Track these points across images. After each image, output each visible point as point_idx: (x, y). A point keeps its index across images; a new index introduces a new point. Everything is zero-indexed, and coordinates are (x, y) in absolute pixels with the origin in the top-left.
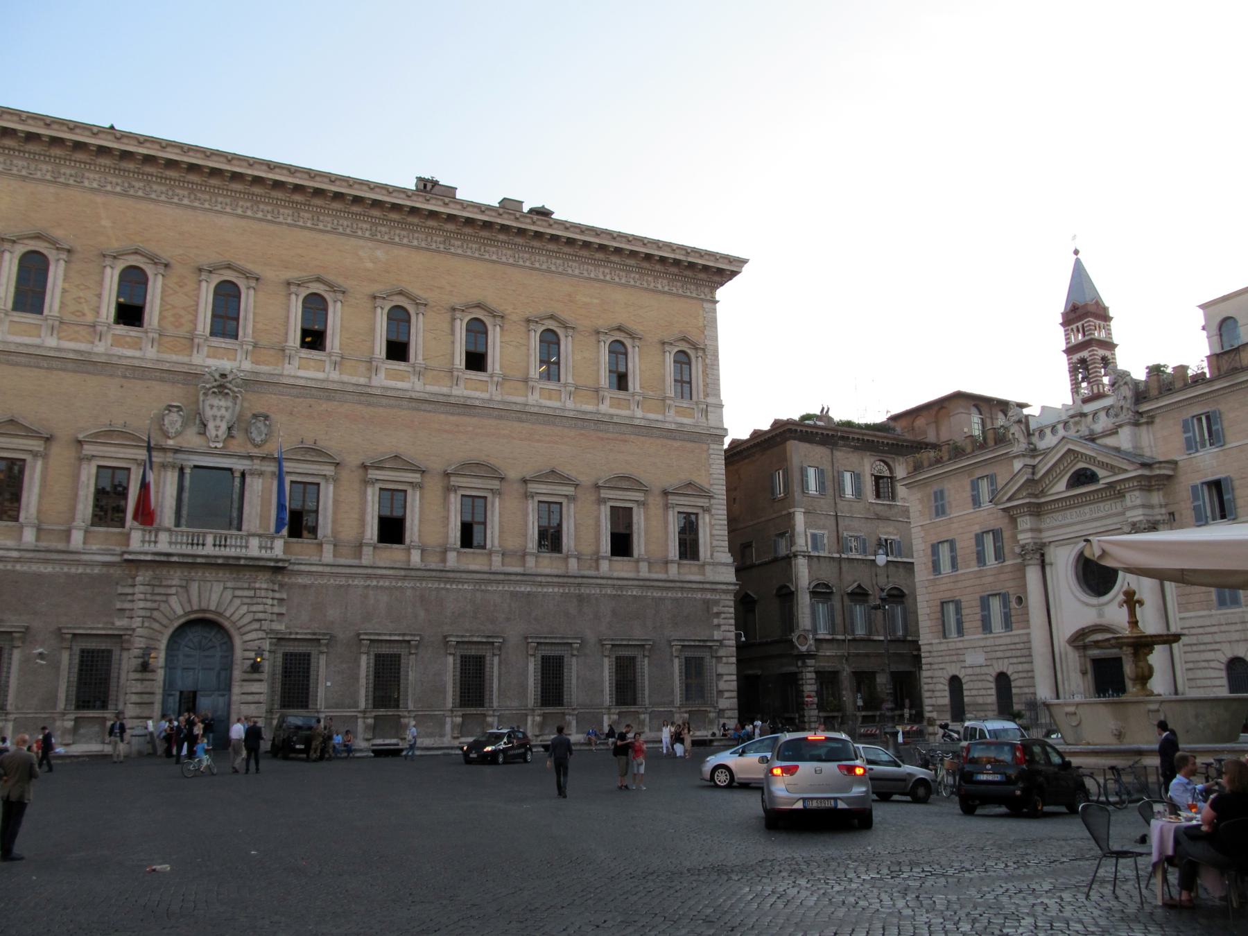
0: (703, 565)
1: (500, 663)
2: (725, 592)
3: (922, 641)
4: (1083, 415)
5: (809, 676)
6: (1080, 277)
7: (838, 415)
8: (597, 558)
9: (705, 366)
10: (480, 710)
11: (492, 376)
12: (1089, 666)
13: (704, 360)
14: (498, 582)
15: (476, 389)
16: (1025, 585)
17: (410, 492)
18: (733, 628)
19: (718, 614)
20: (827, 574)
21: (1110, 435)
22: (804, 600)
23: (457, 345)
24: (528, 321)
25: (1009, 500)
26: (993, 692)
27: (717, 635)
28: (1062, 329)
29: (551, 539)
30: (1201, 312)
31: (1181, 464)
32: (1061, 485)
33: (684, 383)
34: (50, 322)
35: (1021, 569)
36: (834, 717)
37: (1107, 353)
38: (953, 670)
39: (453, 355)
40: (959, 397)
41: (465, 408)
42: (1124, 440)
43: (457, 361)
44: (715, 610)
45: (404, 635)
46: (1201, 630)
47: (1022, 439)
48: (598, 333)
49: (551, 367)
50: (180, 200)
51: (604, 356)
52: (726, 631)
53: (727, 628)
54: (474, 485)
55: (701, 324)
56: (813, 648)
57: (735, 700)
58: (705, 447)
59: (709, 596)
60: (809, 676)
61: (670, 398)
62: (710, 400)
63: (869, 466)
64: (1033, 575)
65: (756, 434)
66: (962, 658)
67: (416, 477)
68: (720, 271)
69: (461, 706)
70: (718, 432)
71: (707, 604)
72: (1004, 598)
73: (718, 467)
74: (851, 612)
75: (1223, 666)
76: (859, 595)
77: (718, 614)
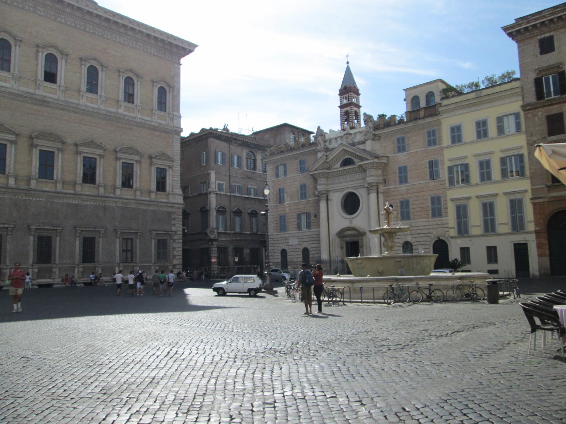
1: (60, 240)
2: (178, 208)
3: (270, 233)
4: (350, 134)
5: (214, 249)
6: (348, 75)
7: (233, 129)
8: (115, 188)
9: (173, 96)
10: (49, 265)
11: (59, 86)
12: (344, 245)
13: (173, 93)
14: (60, 198)
15: (50, 93)
16: (319, 209)
17: (9, 145)
18: (181, 226)
19: (174, 219)
20: (225, 203)
21: (361, 144)
22: (213, 214)
23: (40, 66)
24: (81, 59)
25: (315, 170)
26: (301, 256)
27: (174, 229)
28: (339, 97)
29: (89, 176)
30: (404, 93)
31: (390, 158)
32: (338, 165)
33: (162, 105)
35: (317, 202)
36: (224, 268)
37: (357, 109)
38: (283, 247)
39: (37, 72)
40: (285, 125)
41: (44, 102)
42: (369, 146)
43: (39, 76)
44: (173, 216)
45: (4, 224)
46: (424, 228)
47: (322, 143)
48: (119, 71)
51: (122, 85)
52: (178, 227)
53: (178, 225)
54: (47, 145)
56: (217, 236)
57: (181, 260)
60: (214, 249)
61: (155, 110)
62: (175, 113)
63: (244, 153)
64: (323, 205)
65: (192, 134)
66: (287, 241)
67: (12, 137)
68: (184, 49)
69: (38, 263)
70: (178, 130)
71: (169, 213)
72: (308, 215)
73: (177, 147)
74: (234, 221)
75: (401, 245)
76: (238, 213)
77: (174, 219)
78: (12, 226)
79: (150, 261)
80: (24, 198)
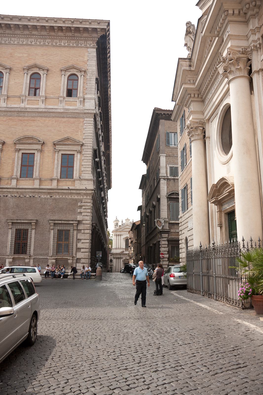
0: (75, 181)
2: (86, 194)
19: (81, 207)
27: (79, 218)
30: (198, 7)
34: (42, 98)
49: (34, 90)
54: (67, 149)
55: (86, 59)
58: (81, 120)
59: (76, 197)
77: (81, 207)
78: (35, 221)
79: (47, 254)
80: (45, 196)
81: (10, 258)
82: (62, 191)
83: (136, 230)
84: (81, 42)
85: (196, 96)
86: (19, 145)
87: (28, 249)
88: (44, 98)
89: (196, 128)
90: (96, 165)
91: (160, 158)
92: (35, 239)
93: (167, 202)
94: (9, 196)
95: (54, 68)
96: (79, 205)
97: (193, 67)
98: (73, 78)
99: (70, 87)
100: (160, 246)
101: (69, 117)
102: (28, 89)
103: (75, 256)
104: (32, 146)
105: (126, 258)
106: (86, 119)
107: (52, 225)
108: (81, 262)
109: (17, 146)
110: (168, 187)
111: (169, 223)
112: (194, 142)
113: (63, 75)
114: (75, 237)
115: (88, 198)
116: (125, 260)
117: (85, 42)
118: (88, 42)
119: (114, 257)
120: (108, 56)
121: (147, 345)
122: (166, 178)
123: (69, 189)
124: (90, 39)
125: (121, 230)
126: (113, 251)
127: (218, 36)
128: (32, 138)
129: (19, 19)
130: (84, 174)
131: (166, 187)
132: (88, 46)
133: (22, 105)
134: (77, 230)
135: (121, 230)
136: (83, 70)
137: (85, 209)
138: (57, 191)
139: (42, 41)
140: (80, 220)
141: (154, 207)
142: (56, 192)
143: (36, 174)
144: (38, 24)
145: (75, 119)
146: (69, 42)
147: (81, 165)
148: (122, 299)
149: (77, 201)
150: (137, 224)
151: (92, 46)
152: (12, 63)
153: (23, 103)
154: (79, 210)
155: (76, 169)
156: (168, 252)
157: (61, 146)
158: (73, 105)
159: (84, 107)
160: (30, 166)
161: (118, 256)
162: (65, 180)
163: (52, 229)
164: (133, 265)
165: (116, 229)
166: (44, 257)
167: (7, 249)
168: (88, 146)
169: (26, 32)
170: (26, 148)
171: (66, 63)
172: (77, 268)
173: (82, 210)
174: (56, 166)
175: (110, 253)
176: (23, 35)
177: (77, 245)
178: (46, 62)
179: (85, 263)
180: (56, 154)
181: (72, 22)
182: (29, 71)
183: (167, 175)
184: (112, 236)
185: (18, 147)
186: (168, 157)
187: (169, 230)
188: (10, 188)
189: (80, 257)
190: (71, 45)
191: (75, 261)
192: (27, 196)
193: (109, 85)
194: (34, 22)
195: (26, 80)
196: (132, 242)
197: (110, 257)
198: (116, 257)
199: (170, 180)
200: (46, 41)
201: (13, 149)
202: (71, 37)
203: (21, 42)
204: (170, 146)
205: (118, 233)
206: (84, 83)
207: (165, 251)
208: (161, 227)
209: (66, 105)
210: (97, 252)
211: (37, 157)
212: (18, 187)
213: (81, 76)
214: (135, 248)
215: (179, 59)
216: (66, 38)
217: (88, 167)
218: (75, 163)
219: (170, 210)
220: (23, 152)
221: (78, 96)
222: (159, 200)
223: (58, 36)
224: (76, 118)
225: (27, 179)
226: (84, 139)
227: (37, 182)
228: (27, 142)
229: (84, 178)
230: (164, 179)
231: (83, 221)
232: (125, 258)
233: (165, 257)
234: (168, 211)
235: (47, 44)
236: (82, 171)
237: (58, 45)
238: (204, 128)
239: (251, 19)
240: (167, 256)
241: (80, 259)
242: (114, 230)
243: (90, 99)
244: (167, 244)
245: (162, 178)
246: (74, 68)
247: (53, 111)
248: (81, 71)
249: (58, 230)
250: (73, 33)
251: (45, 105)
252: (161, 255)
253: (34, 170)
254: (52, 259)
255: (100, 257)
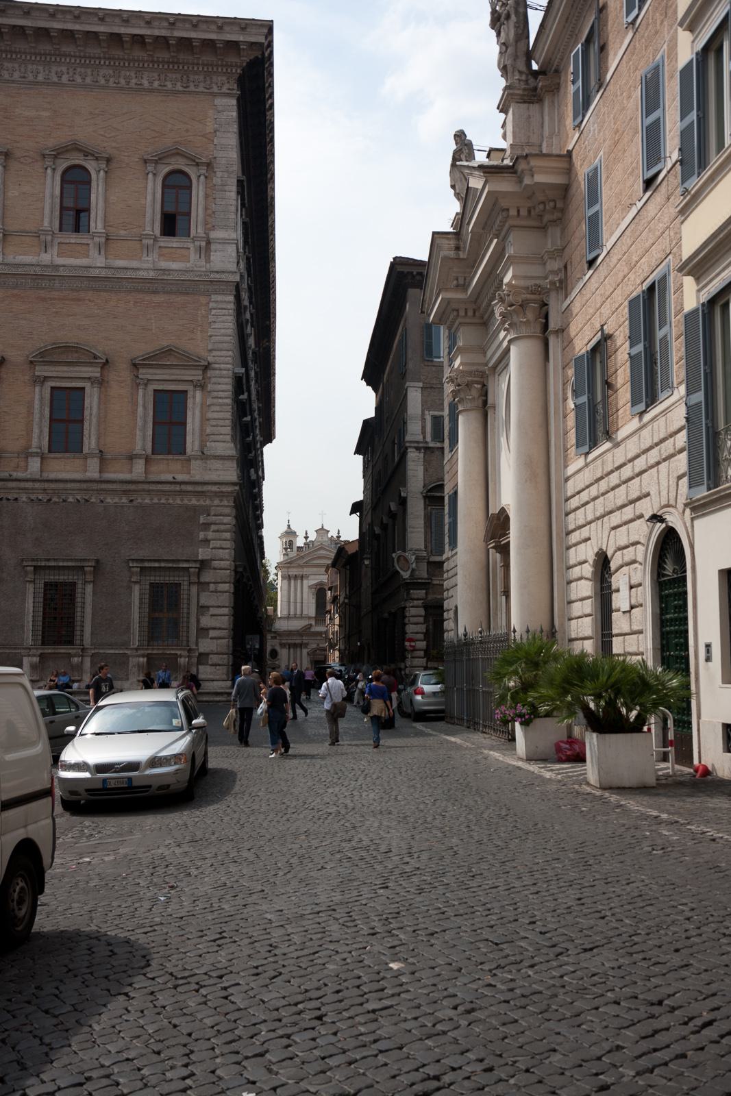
0: (189, 460)
19: (206, 526)
27: (203, 553)
34: (97, 240)
49: (75, 216)
50: (220, 88)
54: (165, 379)
55: (210, 129)
58: (203, 300)
59: (194, 502)
77: (206, 526)
79: (125, 644)
80: (116, 500)
81: (34, 656)
82: (160, 486)
83: (348, 567)
84: (197, 77)
85: (470, 313)
86: (43, 367)
87: (78, 633)
88: (103, 240)
89: (469, 385)
90: (241, 408)
91: (406, 394)
92: (94, 607)
93: (425, 509)
94: (24, 499)
95: (126, 154)
96: (201, 522)
97: (464, 251)
98: (177, 184)
99: (170, 209)
100: (406, 620)
101: (171, 293)
102: (57, 213)
103: (194, 647)
104: (77, 369)
105: (318, 645)
106: (214, 298)
107: (137, 572)
108: (210, 663)
109: (37, 368)
110: (426, 470)
111: (429, 563)
112: (464, 413)
113: (150, 176)
114: (194, 601)
115: (225, 503)
116: (314, 651)
117: (208, 78)
118: (214, 78)
119: (283, 641)
120: (267, 106)
121: (390, 916)
122: (421, 445)
123: (175, 483)
124: (220, 70)
125: (301, 562)
126: (281, 625)
127: (497, 236)
128: (75, 349)
129: (25, 12)
130: (213, 444)
131: (421, 469)
132: (215, 89)
133: (45, 258)
134: (199, 583)
135: (301, 562)
136: (204, 160)
137: (218, 531)
138: (146, 487)
139: (89, 71)
140: (206, 560)
141: (393, 516)
142: (144, 490)
143: (90, 442)
144: (77, 27)
145: (186, 298)
146: (162, 77)
147: (204, 420)
148: (315, 735)
149: (196, 511)
150: (351, 550)
151: (224, 90)
152: (9, 137)
153: (46, 252)
154: (202, 535)
155: (193, 429)
156: (426, 634)
157: (151, 371)
158: (179, 259)
159: (208, 265)
160: (75, 421)
161: (295, 640)
162: (163, 459)
163: (135, 582)
164: (338, 668)
165: (286, 557)
166: (117, 652)
167: (24, 632)
168: (220, 370)
169: (45, 47)
170: (61, 374)
171: (157, 139)
172: (201, 676)
173: (211, 533)
174: (140, 422)
175: (270, 631)
176: (35, 54)
177: (520, 759)
178: (102, 135)
179: (219, 665)
180: (141, 392)
181: (170, 23)
182: (59, 161)
183: (424, 438)
184: (276, 578)
185: (41, 371)
186: (429, 390)
187: (428, 579)
188: (27, 480)
189: (207, 650)
190: (169, 85)
191: (194, 660)
192: (71, 499)
193: (269, 176)
194: (65, 22)
195: (52, 186)
196: (335, 599)
197: (271, 643)
198: (290, 641)
199: (433, 452)
200: (101, 74)
201: (27, 377)
202: (168, 63)
203: (30, 75)
204: (435, 360)
205: (293, 572)
206: (207, 196)
207: (417, 633)
208: (409, 572)
209: (162, 258)
210: (248, 637)
211: (92, 398)
212: (45, 475)
213: (200, 176)
214: (345, 617)
215: (434, 233)
216: (156, 66)
217: (222, 424)
218: (189, 414)
219: (431, 528)
220: (53, 384)
221: (193, 233)
222: (403, 502)
223: (134, 61)
224: (188, 294)
225: (67, 455)
226: (210, 351)
227: (94, 464)
228: (64, 358)
229: (213, 452)
230: (418, 449)
231: (213, 562)
232: (314, 646)
233: (417, 647)
234: (426, 533)
235: (103, 82)
236: (208, 435)
237: (134, 86)
238: (484, 385)
239: (550, 228)
240: (423, 645)
241: (207, 654)
242: (281, 563)
243: (225, 242)
244: (423, 614)
245: (413, 445)
246: (178, 154)
247: (129, 274)
248: (197, 163)
249: (151, 584)
250: (172, 54)
251: (106, 259)
252: (407, 644)
253: (86, 433)
254: (139, 656)
255: (255, 649)
